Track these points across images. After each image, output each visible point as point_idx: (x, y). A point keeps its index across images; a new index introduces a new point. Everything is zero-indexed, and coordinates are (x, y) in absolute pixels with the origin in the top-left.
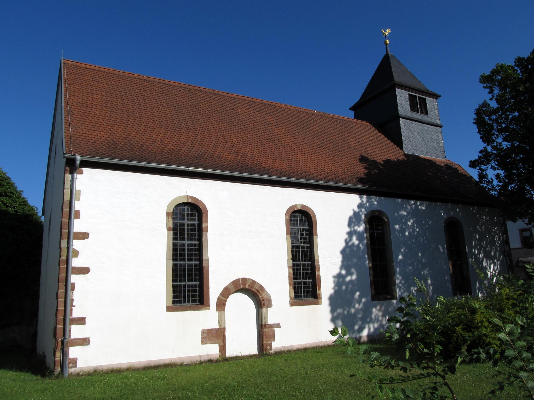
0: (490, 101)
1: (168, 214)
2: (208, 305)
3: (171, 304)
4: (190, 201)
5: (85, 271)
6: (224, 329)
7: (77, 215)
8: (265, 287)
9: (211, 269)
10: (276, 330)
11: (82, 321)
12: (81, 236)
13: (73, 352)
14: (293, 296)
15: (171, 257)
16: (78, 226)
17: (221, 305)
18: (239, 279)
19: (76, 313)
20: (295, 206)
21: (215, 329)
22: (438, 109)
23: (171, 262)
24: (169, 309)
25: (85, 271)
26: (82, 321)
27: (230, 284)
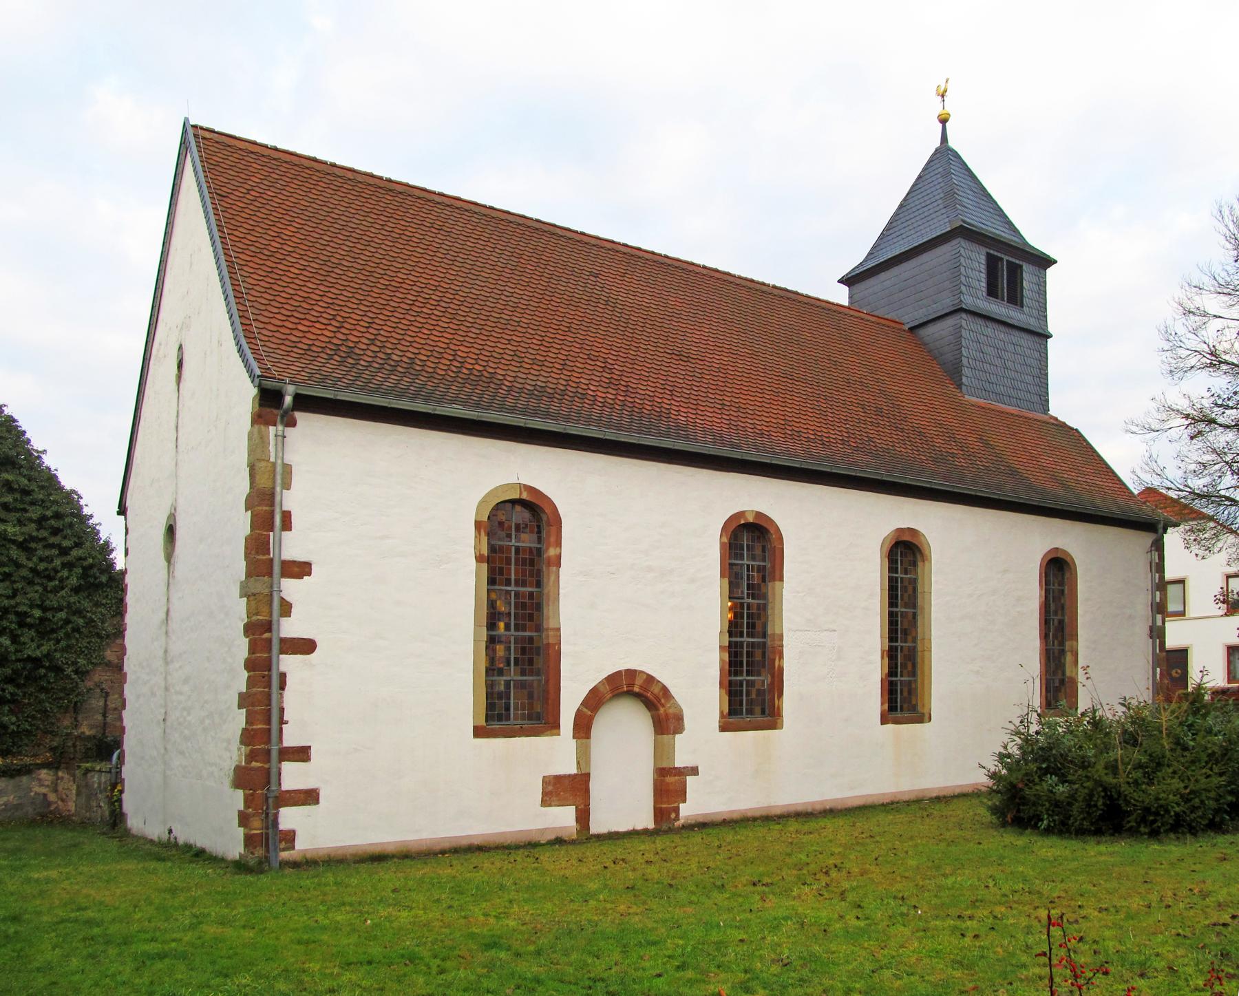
1: (478, 525)
4: (525, 496)
5: (306, 646)
6: (588, 775)
8: (673, 691)
9: (565, 648)
10: (690, 780)
11: (302, 754)
14: (726, 710)
17: (583, 727)
20: (741, 514)
24: (479, 732)
25: (306, 646)
26: (302, 754)
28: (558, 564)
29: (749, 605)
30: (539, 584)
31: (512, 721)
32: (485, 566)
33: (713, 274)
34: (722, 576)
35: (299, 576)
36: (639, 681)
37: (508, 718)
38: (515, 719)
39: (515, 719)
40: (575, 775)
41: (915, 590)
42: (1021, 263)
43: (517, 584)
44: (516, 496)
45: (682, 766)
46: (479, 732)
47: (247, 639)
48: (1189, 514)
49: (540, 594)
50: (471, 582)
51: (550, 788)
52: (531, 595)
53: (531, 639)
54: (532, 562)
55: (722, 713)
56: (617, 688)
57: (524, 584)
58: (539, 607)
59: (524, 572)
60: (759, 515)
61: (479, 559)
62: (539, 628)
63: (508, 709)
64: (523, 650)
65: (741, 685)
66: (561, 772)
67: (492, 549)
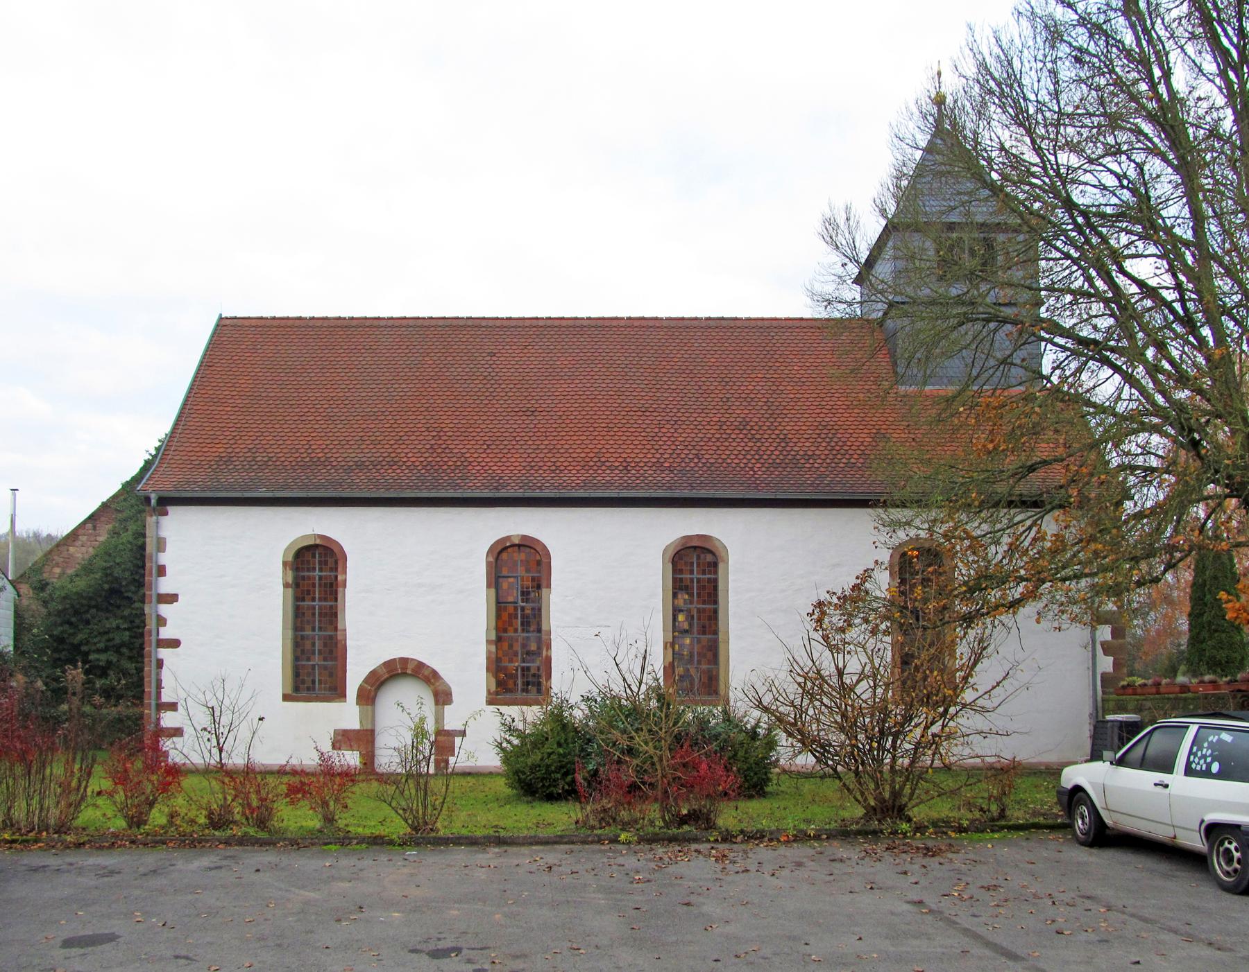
0: (818, 226)
1: (285, 564)
2: (344, 696)
3: (289, 691)
4: (318, 542)
5: (175, 643)
6: (372, 732)
7: (162, 571)
8: (442, 673)
9: (350, 643)
10: (458, 740)
11: (173, 707)
12: (316, 636)
13: (167, 744)
14: (493, 688)
15: (290, 625)
16: (165, 585)
17: (368, 696)
18: (395, 659)
19: (166, 697)
20: (508, 538)
21: (354, 730)
22: (1050, 320)
23: (290, 633)
24: (286, 698)
25: (175, 643)
26: (173, 707)
27: (445, 682)
28: (345, 586)
29: (523, 609)
30: (336, 600)
31: (317, 692)
32: (290, 590)
33: (376, 323)
34: (488, 586)
35: (171, 602)
36: (411, 666)
37: (314, 689)
38: (320, 689)
39: (320, 689)
40: (358, 731)
41: (715, 588)
42: (1115, 641)
43: (320, 599)
44: (312, 542)
45: (450, 729)
46: (286, 698)
47: (1098, 627)
48: (1188, 271)
49: (336, 607)
50: (279, 601)
51: (340, 738)
52: (331, 607)
53: (331, 637)
54: (331, 585)
55: (489, 692)
56: (392, 671)
57: (326, 600)
58: (336, 615)
59: (326, 592)
60: (524, 537)
61: (286, 585)
62: (336, 629)
63: (313, 682)
64: (325, 645)
65: (517, 670)
66: (349, 727)
67: (296, 578)
